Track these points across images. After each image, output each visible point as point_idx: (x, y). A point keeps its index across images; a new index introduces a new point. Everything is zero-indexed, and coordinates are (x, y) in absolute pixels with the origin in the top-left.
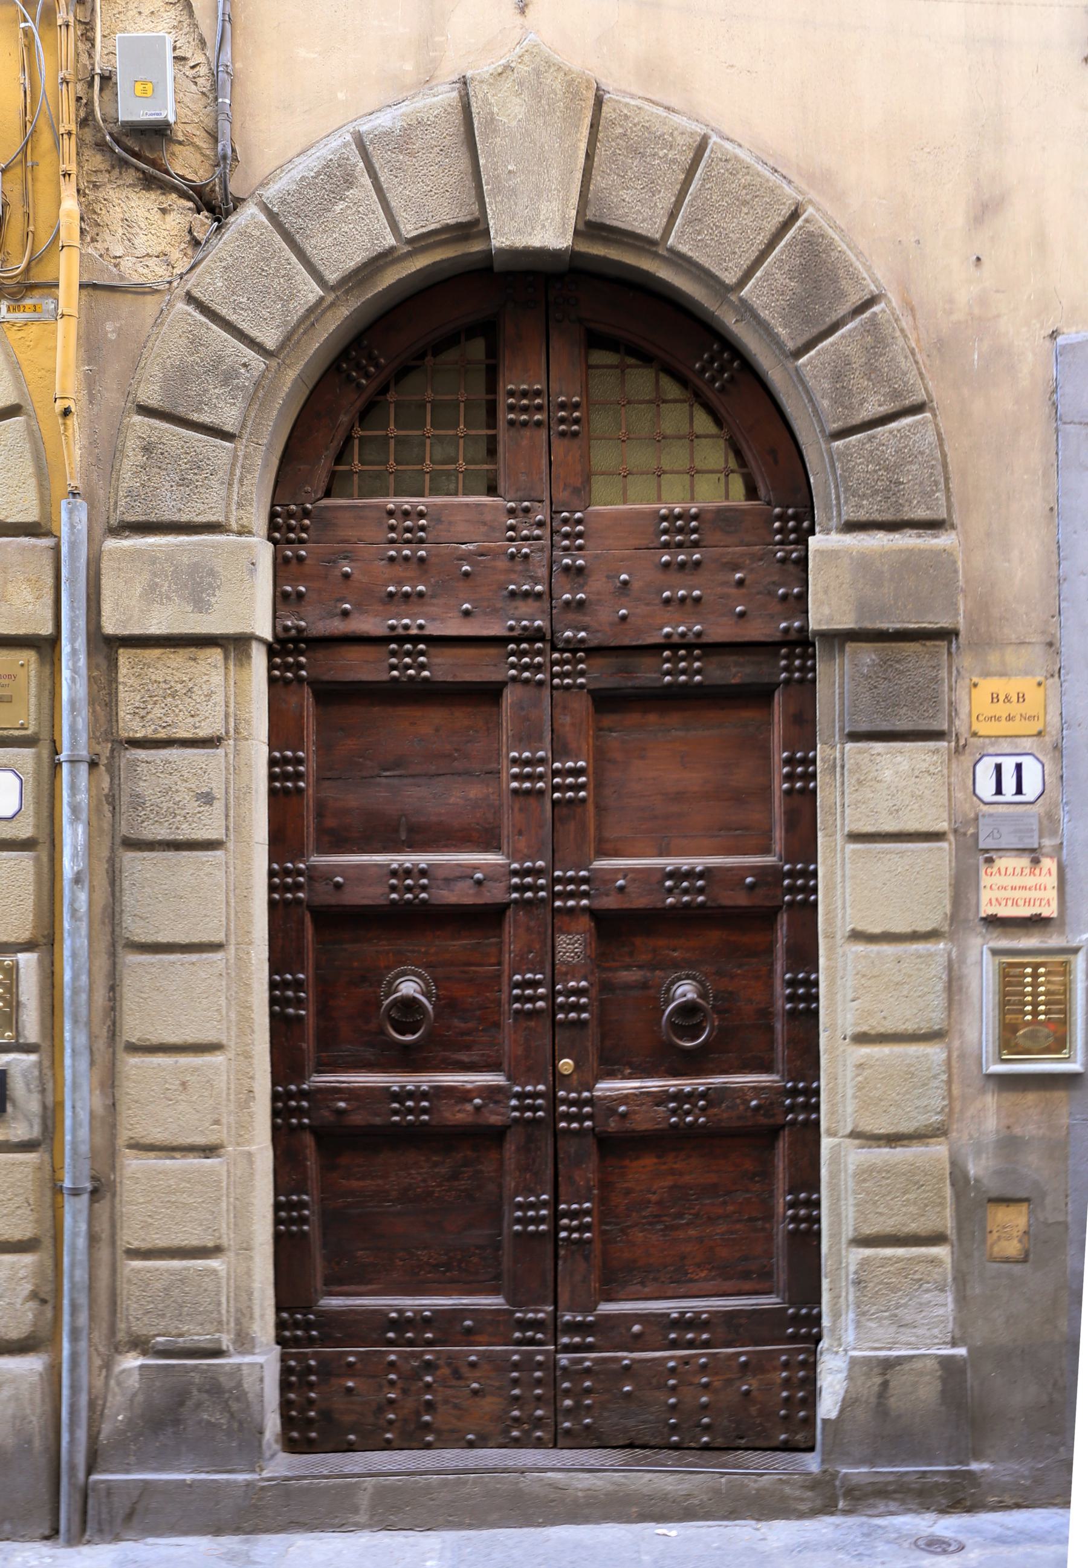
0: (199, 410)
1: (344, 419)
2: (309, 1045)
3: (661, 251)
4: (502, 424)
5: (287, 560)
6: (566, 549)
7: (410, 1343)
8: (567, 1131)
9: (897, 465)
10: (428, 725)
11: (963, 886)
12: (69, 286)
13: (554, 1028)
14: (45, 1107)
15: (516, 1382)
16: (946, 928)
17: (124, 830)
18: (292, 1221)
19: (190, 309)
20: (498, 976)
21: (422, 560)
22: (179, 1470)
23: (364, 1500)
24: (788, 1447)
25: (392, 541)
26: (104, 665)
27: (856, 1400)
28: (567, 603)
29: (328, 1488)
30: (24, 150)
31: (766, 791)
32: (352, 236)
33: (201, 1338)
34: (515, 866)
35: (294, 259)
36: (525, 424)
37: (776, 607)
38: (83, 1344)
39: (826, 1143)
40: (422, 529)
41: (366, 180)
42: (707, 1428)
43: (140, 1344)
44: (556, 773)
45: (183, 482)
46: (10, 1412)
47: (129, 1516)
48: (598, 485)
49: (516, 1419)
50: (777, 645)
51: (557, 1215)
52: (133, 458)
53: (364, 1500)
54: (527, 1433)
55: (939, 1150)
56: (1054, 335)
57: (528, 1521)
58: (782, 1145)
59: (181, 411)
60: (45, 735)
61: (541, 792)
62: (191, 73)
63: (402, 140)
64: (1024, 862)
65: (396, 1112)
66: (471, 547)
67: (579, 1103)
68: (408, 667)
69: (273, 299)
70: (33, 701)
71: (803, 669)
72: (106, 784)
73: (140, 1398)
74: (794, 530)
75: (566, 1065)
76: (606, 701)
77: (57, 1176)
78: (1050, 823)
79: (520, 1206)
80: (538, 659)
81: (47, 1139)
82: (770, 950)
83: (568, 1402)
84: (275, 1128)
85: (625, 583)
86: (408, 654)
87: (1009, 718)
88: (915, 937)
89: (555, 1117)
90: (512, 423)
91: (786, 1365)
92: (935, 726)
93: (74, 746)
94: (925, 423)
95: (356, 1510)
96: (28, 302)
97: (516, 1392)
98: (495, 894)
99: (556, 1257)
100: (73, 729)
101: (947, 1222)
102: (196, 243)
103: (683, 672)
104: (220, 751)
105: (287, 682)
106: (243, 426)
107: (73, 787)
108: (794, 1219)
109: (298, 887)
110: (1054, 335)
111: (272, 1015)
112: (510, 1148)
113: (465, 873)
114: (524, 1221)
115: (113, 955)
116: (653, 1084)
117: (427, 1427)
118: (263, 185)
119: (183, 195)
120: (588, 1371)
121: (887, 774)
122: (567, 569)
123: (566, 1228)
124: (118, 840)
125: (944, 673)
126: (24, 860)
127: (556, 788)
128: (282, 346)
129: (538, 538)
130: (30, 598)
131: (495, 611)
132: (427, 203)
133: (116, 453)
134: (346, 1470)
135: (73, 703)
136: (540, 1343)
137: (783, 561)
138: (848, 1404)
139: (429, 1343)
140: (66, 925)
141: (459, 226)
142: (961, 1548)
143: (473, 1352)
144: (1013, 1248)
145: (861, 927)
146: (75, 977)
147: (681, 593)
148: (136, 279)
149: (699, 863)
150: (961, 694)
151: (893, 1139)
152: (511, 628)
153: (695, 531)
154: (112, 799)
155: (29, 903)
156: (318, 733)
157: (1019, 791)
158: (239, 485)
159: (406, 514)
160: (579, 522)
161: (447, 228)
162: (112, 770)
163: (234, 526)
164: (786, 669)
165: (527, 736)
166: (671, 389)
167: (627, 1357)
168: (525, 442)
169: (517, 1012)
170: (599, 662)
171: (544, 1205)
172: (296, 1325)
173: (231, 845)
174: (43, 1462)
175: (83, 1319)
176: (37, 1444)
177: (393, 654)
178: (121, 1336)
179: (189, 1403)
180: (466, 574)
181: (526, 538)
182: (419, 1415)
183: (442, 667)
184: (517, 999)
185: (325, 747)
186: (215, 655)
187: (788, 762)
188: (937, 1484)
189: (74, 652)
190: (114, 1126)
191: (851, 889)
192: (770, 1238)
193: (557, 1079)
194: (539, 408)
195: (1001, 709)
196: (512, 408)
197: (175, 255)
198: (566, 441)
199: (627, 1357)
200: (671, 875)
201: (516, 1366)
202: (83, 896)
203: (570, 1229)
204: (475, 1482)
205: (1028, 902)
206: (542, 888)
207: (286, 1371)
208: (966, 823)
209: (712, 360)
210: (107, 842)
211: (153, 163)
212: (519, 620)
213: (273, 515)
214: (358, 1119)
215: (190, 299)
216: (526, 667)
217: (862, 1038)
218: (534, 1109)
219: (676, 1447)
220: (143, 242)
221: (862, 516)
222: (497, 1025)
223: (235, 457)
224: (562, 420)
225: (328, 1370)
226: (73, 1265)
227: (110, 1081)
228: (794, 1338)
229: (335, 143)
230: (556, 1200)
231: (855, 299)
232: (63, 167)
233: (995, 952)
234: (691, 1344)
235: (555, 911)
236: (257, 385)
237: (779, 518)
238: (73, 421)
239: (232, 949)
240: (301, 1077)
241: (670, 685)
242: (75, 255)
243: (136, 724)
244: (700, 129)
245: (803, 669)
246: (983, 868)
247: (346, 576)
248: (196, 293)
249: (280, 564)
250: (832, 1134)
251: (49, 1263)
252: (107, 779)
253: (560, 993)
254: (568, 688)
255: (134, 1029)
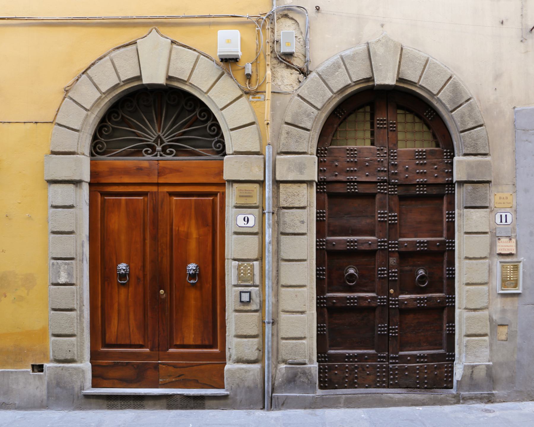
0: (301, 123)
1: (336, 126)
2: (326, 286)
3: (418, 85)
4: (375, 128)
5: (321, 161)
6: (392, 159)
7: (351, 362)
8: (392, 308)
9: (477, 139)
10: (357, 203)
11: (492, 245)
12: (269, 92)
13: (389, 282)
14: (260, 301)
15: (378, 372)
16: (488, 256)
17: (281, 230)
18: (321, 331)
19: (299, 98)
20: (374, 268)
21: (356, 162)
22: (295, 393)
23: (342, 401)
24: (446, 388)
25: (348, 157)
26: (276, 188)
27: (465, 376)
28: (393, 173)
29: (333, 398)
30: (257, 59)
31: (441, 221)
32: (340, 81)
33: (301, 360)
34: (379, 240)
35: (325, 86)
36: (381, 128)
37: (445, 175)
38: (270, 362)
39: (457, 311)
40: (356, 154)
41: (343, 67)
42: (426, 383)
43: (285, 362)
44: (390, 216)
45: (297, 141)
46: (252, 378)
47: (283, 404)
48: (400, 143)
49: (378, 381)
50: (445, 184)
51: (389, 329)
52: (284, 135)
53: (342, 401)
54: (381, 385)
55: (486, 312)
56: (514, 108)
57: (383, 406)
58: (445, 312)
59: (296, 124)
60: (261, 206)
61: (386, 221)
62: (298, 40)
63: (353, 57)
64: (507, 239)
65: (348, 303)
66: (368, 159)
67: (395, 301)
68: (352, 189)
69: (322, 96)
70: (258, 197)
71: (451, 190)
72: (276, 218)
73: (285, 375)
74: (449, 155)
75: (392, 291)
76: (402, 198)
77: (264, 318)
78: (514, 230)
79: (380, 327)
80: (385, 187)
81: (261, 309)
82: (442, 262)
83: (392, 377)
84: (317, 307)
85: (407, 168)
86: (352, 185)
87: (504, 203)
88: (481, 258)
89: (389, 304)
90: (378, 127)
91: (446, 367)
92: (486, 205)
93: (269, 209)
94: (483, 129)
95: (340, 403)
96: (257, 96)
97: (379, 374)
98: (374, 247)
99: (389, 340)
100: (269, 204)
101: (488, 331)
102: (300, 82)
103: (422, 191)
104: (306, 210)
105: (321, 192)
106: (312, 128)
107: (269, 219)
108: (448, 330)
109: (324, 245)
110: (514, 108)
111: (317, 278)
112: (377, 312)
113: (366, 242)
114: (381, 331)
115: (278, 262)
116: (413, 296)
117: (356, 383)
118: (317, 68)
119: (296, 70)
120: (397, 369)
121: (474, 217)
122: (393, 164)
123: (391, 333)
124: (279, 233)
125: (488, 192)
126: (256, 238)
127: (390, 220)
128: (322, 108)
129: (385, 156)
130: (258, 170)
131: (374, 175)
132: (359, 73)
133: (279, 134)
134: (338, 393)
135: (269, 198)
136: (384, 362)
137: (447, 163)
138: (463, 376)
139: (356, 362)
140: (267, 254)
141: (367, 79)
142: (494, 411)
143: (368, 364)
144: (504, 337)
145: (467, 256)
146: (269, 268)
147: (421, 171)
148: (284, 91)
149: (425, 239)
150: (492, 197)
151: (475, 310)
152: (379, 179)
153: (424, 155)
154: (278, 223)
155: (257, 249)
156: (328, 205)
157: (506, 222)
158: (309, 142)
159: (351, 150)
160: (395, 153)
161: (364, 79)
162: (277, 214)
163: (310, 153)
164: (447, 190)
165: (382, 207)
166: (417, 120)
167: (406, 365)
168: (382, 132)
169: (379, 277)
170: (401, 188)
171: (386, 327)
172: (322, 357)
173: (308, 234)
174: (260, 390)
175: (270, 355)
176: (259, 386)
177: (348, 185)
178: (280, 359)
179: (298, 376)
180: (367, 165)
181: (382, 157)
182: (353, 380)
183: (359, 189)
184: (380, 274)
185: (330, 209)
186: (305, 185)
187: (447, 214)
188: (485, 397)
189: (269, 184)
190: (278, 306)
191: (463, 246)
192: (442, 335)
193: (389, 295)
194: (385, 124)
195: (502, 201)
196: (378, 124)
197: (294, 85)
198: (392, 132)
199: (406, 365)
200: (418, 243)
201: (378, 368)
202: (271, 247)
203: (392, 333)
204: (370, 396)
205: (508, 250)
206: (386, 246)
207: (320, 369)
208: (493, 230)
209: (428, 113)
210: (276, 233)
211: (289, 62)
212: (380, 177)
213: (317, 150)
214: (338, 305)
215: (299, 96)
216: (382, 189)
217: (468, 284)
218: (384, 302)
219: (418, 388)
220: (286, 81)
221: (468, 152)
222: (374, 281)
223: (310, 135)
224: (391, 127)
225: (331, 368)
226: (268, 341)
227: (277, 295)
228: (448, 360)
229: (335, 58)
230: (389, 326)
231: (466, 98)
232: (267, 63)
233: (501, 262)
234: (422, 362)
235: (389, 251)
236: (316, 117)
237: (445, 152)
238: (269, 126)
239: (308, 260)
240: (324, 294)
241: (418, 194)
242: (270, 84)
243: (284, 203)
244: (427, 56)
245: (451, 190)
246: (497, 240)
247: (336, 166)
248: (300, 94)
249: (319, 162)
250: (459, 308)
251: (261, 341)
252: (276, 217)
253: (390, 273)
254: (393, 194)
255: (283, 281)
